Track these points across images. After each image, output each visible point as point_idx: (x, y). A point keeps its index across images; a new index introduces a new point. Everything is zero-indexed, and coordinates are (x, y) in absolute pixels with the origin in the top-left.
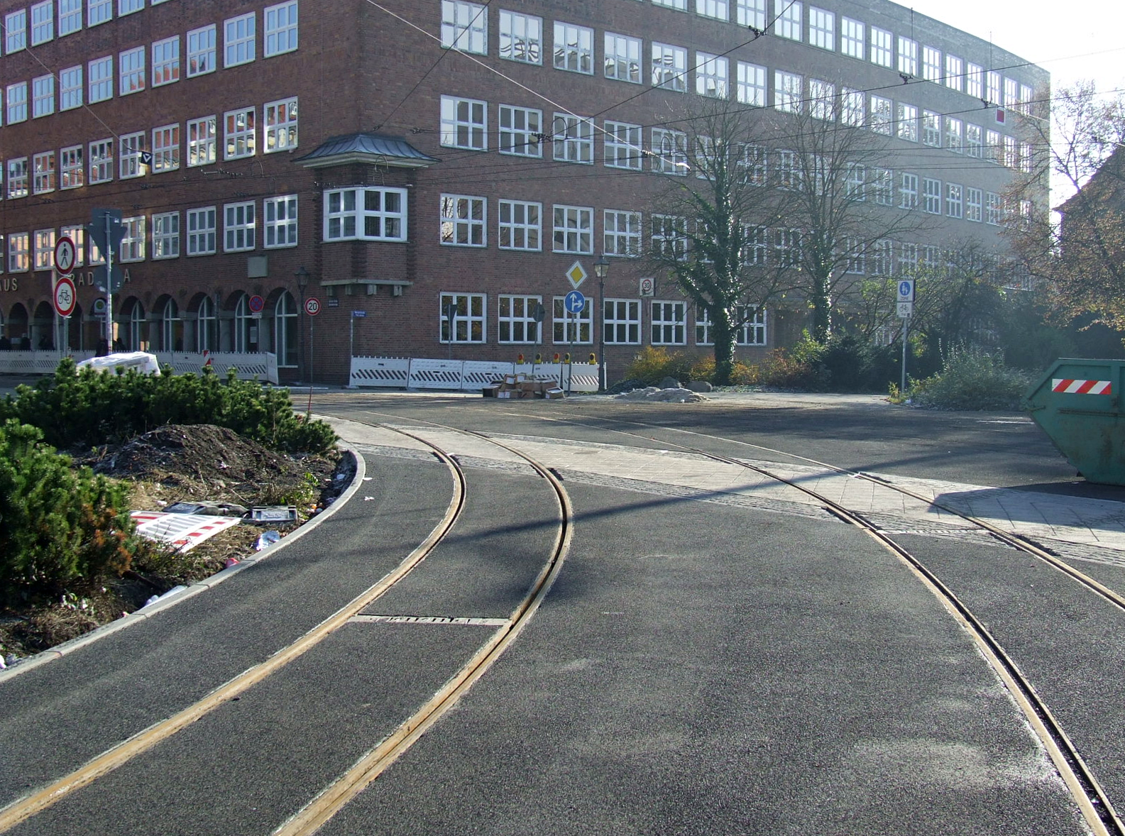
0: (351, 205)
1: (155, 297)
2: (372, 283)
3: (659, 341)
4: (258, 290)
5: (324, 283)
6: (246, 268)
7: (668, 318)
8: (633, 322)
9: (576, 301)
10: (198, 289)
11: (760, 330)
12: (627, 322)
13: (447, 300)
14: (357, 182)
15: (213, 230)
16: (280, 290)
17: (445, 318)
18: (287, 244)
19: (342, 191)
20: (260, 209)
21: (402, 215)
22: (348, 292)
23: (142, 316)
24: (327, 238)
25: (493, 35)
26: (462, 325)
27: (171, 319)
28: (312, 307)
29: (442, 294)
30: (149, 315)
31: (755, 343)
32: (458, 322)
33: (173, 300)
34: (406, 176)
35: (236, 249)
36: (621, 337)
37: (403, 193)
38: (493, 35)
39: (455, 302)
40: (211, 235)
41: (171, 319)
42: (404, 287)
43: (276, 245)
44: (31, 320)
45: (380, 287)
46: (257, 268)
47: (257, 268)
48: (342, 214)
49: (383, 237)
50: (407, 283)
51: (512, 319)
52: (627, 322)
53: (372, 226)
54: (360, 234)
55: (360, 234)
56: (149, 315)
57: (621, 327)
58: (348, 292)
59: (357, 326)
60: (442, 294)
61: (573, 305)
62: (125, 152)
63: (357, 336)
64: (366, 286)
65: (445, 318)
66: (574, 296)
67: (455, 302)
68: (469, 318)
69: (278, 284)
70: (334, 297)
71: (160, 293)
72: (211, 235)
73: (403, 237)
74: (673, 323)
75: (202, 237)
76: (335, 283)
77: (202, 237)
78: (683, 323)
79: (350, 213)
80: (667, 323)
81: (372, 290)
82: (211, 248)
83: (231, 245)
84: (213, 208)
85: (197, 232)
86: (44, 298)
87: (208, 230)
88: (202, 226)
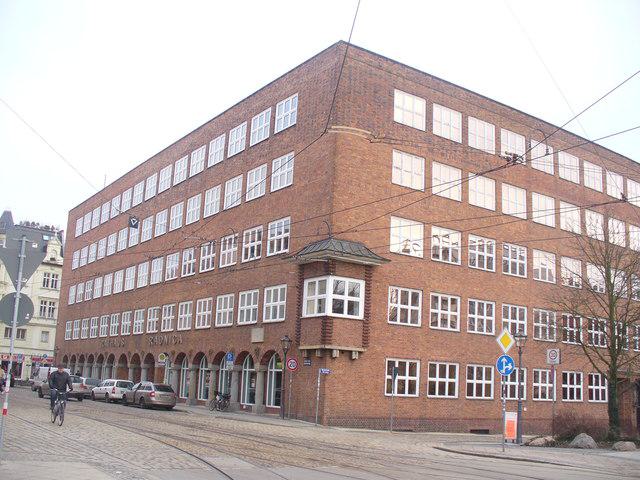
0: (323, 291)
1: (194, 354)
2: (336, 347)
3: (481, 395)
4: (257, 351)
5: (301, 348)
6: (250, 336)
7: (442, 375)
8: (452, 380)
9: (507, 364)
10: (220, 349)
11: (488, 387)
12: (447, 380)
13: (391, 364)
14: (328, 273)
15: (256, 306)
16: (272, 352)
17: (390, 377)
18: (278, 319)
19: (317, 280)
20: (262, 295)
21: (361, 300)
22: (318, 354)
23: (252, 366)
24: (305, 315)
25: (428, 178)
26: (402, 383)
27: (248, 370)
28: (292, 364)
29: (388, 359)
30: (210, 366)
31: (575, 400)
32: (399, 381)
33: (251, 356)
34: (367, 272)
35: (245, 322)
36: (442, 392)
37: (362, 283)
38: (428, 178)
39: (397, 366)
40: (209, 315)
41: (204, 369)
42: (360, 353)
43: (271, 320)
44: (129, 365)
45: (342, 352)
46: (257, 336)
47: (257, 336)
48: (317, 296)
49: (345, 315)
50: (363, 350)
51: (437, 380)
52: (447, 380)
53: (338, 307)
54: (329, 312)
55: (329, 312)
56: (257, 366)
57: (572, 390)
58: (318, 354)
59: (323, 380)
60: (388, 359)
61: (505, 367)
62: (247, 242)
63: (323, 387)
64: (331, 351)
65: (390, 377)
66: (504, 360)
67: (397, 366)
68: (407, 378)
69: (270, 347)
70: (308, 358)
71: (198, 351)
72: (255, 310)
73: (361, 316)
74: (516, 383)
75: (275, 308)
76: (309, 348)
77: (225, 314)
78: (581, 387)
79: (322, 296)
80: (571, 386)
81: (336, 354)
82: (281, 316)
83: (242, 320)
84: (233, 295)
85: (202, 313)
86: (137, 351)
87: (253, 306)
88: (225, 308)
